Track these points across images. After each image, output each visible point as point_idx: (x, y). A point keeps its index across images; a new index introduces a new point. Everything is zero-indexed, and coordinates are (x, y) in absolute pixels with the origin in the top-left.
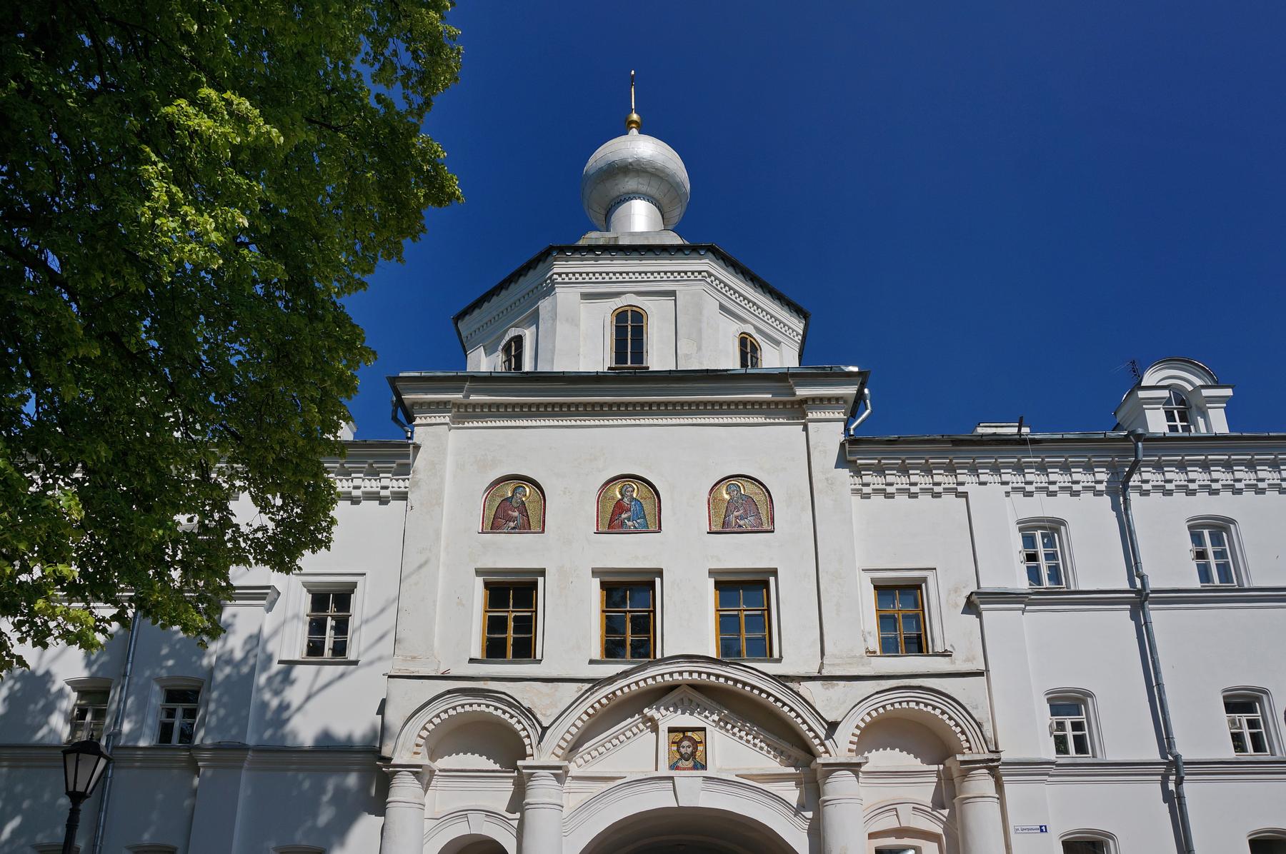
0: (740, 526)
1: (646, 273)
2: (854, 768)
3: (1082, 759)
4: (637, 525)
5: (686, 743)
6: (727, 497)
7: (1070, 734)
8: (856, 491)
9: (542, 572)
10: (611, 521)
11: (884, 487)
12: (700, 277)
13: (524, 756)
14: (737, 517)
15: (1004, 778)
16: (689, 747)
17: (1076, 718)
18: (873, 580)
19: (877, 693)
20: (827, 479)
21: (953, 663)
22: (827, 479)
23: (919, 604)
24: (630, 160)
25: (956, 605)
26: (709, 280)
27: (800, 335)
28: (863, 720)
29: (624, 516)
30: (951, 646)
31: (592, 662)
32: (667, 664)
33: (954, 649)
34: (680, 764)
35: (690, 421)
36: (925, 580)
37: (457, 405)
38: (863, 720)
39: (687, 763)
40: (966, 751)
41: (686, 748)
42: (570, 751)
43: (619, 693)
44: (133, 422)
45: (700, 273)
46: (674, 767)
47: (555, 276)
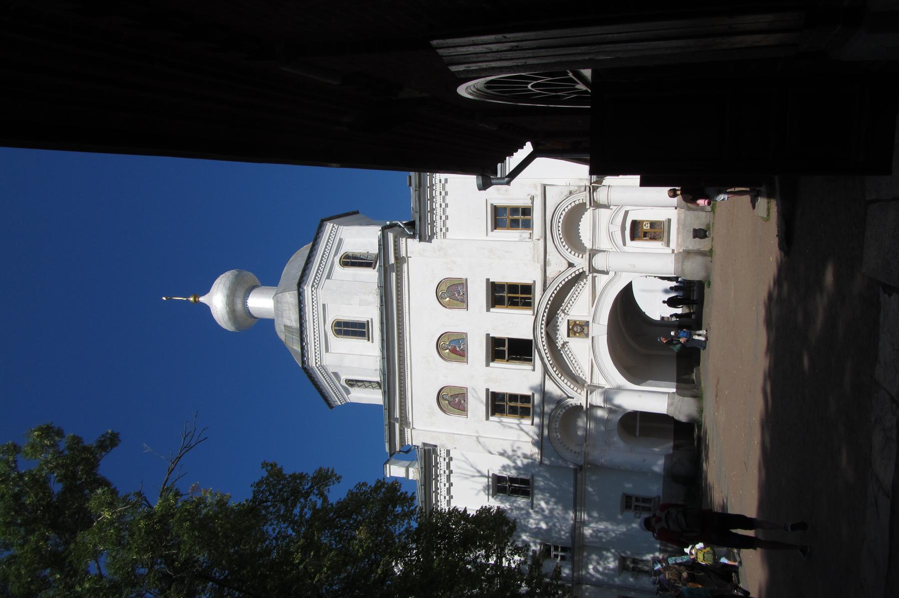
0: (464, 294)
1: (314, 319)
4: (463, 343)
5: (575, 329)
6: (448, 299)
9: (487, 390)
10: (462, 356)
12: (315, 291)
14: (459, 295)
16: (577, 328)
17: (634, 499)
18: (492, 231)
19: (554, 242)
20: (439, 250)
21: (537, 195)
22: (439, 250)
23: (504, 208)
24: (228, 309)
25: (507, 191)
26: (316, 286)
27: (333, 225)
29: (458, 349)
30: (528, 195)
31: (534, 370)
32: (537, 339)
33: (529, 194)
34: (586, 332)
35: (407, 314)
37: (401, 425)
39: (585, 329)
41: (578, 329)
42: (577, 382)
43: (551, 362)
44: (443, 566)
45: (312, 291)
46: (587, 335)
47: (317, 365)
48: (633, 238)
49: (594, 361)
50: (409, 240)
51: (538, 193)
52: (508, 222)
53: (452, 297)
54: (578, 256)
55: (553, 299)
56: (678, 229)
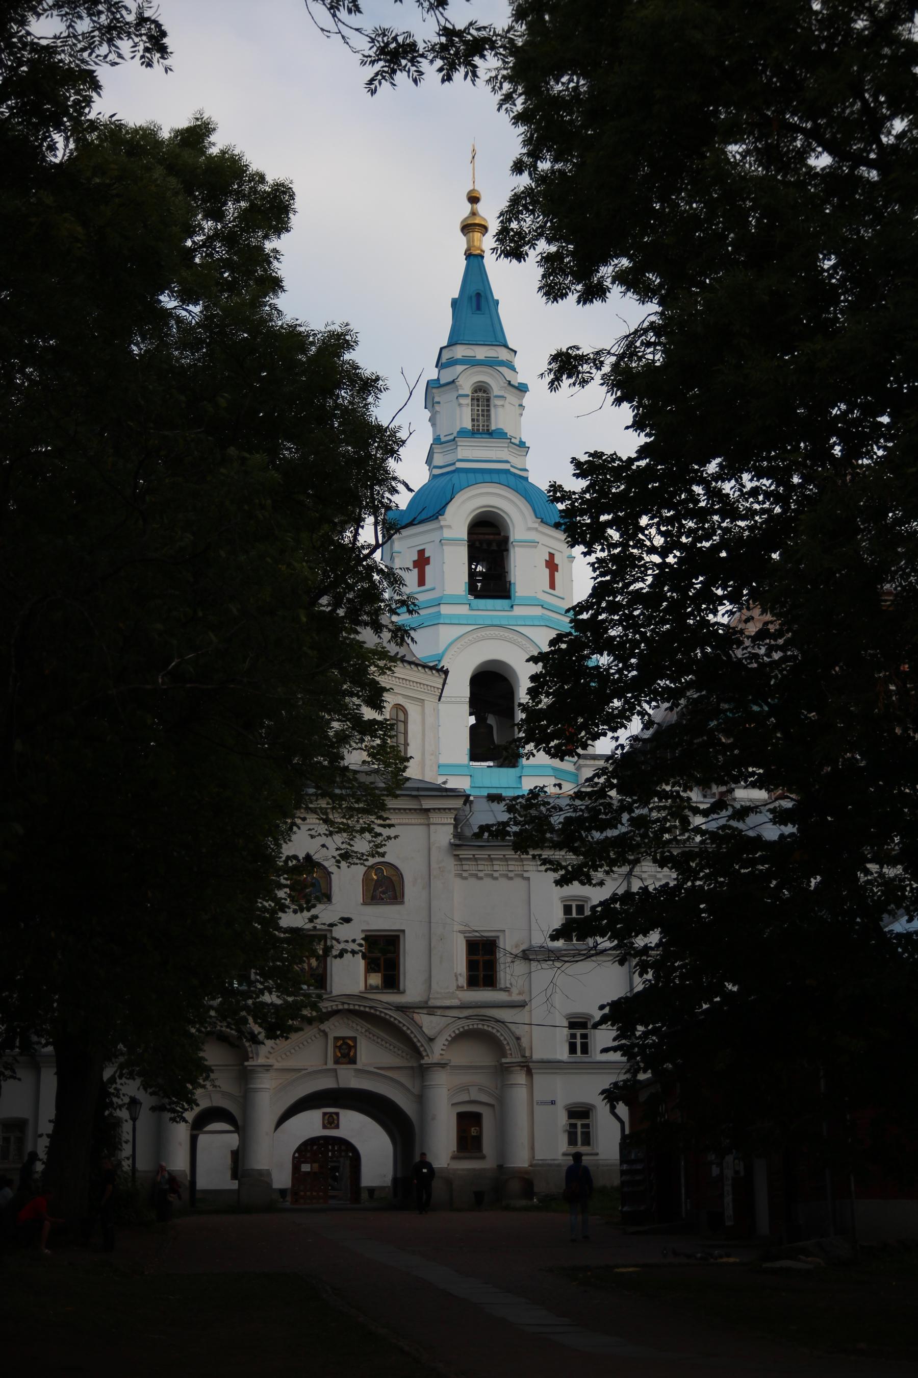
0: (383, 899)
2: (443, 1066)
3: (585, 1058)
5: (344, 1047)
6: (375, 877)
7: (579, 1041)
8: (460, 876)
11: (461, 872)
13: (247, 1060)
14: (381, 892)
15: (533, 1071)
20: (440, 868)
21: (510, 995)
28: (450, 1035)
36: (498, 937)
38: (450, 1035)
40: (509, 1056)
46: (337, 1062)
48: (461, 1116)
49: (304, 1072)
50: (451, 829)
51: (515, 997)
52: (475, 958)
53: (378, 884)
54: (444, 1045)
55: (366, 1012)
56: (474, 1170)
